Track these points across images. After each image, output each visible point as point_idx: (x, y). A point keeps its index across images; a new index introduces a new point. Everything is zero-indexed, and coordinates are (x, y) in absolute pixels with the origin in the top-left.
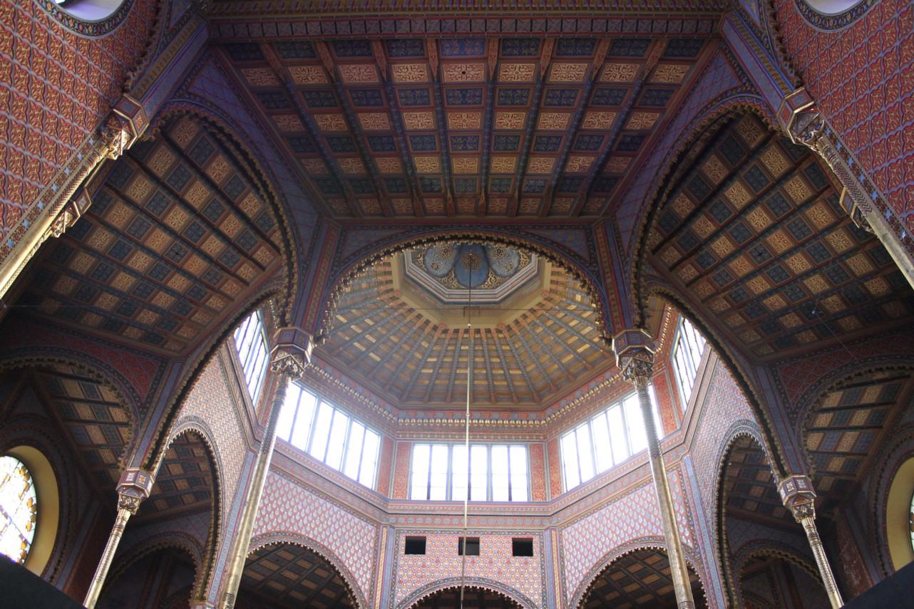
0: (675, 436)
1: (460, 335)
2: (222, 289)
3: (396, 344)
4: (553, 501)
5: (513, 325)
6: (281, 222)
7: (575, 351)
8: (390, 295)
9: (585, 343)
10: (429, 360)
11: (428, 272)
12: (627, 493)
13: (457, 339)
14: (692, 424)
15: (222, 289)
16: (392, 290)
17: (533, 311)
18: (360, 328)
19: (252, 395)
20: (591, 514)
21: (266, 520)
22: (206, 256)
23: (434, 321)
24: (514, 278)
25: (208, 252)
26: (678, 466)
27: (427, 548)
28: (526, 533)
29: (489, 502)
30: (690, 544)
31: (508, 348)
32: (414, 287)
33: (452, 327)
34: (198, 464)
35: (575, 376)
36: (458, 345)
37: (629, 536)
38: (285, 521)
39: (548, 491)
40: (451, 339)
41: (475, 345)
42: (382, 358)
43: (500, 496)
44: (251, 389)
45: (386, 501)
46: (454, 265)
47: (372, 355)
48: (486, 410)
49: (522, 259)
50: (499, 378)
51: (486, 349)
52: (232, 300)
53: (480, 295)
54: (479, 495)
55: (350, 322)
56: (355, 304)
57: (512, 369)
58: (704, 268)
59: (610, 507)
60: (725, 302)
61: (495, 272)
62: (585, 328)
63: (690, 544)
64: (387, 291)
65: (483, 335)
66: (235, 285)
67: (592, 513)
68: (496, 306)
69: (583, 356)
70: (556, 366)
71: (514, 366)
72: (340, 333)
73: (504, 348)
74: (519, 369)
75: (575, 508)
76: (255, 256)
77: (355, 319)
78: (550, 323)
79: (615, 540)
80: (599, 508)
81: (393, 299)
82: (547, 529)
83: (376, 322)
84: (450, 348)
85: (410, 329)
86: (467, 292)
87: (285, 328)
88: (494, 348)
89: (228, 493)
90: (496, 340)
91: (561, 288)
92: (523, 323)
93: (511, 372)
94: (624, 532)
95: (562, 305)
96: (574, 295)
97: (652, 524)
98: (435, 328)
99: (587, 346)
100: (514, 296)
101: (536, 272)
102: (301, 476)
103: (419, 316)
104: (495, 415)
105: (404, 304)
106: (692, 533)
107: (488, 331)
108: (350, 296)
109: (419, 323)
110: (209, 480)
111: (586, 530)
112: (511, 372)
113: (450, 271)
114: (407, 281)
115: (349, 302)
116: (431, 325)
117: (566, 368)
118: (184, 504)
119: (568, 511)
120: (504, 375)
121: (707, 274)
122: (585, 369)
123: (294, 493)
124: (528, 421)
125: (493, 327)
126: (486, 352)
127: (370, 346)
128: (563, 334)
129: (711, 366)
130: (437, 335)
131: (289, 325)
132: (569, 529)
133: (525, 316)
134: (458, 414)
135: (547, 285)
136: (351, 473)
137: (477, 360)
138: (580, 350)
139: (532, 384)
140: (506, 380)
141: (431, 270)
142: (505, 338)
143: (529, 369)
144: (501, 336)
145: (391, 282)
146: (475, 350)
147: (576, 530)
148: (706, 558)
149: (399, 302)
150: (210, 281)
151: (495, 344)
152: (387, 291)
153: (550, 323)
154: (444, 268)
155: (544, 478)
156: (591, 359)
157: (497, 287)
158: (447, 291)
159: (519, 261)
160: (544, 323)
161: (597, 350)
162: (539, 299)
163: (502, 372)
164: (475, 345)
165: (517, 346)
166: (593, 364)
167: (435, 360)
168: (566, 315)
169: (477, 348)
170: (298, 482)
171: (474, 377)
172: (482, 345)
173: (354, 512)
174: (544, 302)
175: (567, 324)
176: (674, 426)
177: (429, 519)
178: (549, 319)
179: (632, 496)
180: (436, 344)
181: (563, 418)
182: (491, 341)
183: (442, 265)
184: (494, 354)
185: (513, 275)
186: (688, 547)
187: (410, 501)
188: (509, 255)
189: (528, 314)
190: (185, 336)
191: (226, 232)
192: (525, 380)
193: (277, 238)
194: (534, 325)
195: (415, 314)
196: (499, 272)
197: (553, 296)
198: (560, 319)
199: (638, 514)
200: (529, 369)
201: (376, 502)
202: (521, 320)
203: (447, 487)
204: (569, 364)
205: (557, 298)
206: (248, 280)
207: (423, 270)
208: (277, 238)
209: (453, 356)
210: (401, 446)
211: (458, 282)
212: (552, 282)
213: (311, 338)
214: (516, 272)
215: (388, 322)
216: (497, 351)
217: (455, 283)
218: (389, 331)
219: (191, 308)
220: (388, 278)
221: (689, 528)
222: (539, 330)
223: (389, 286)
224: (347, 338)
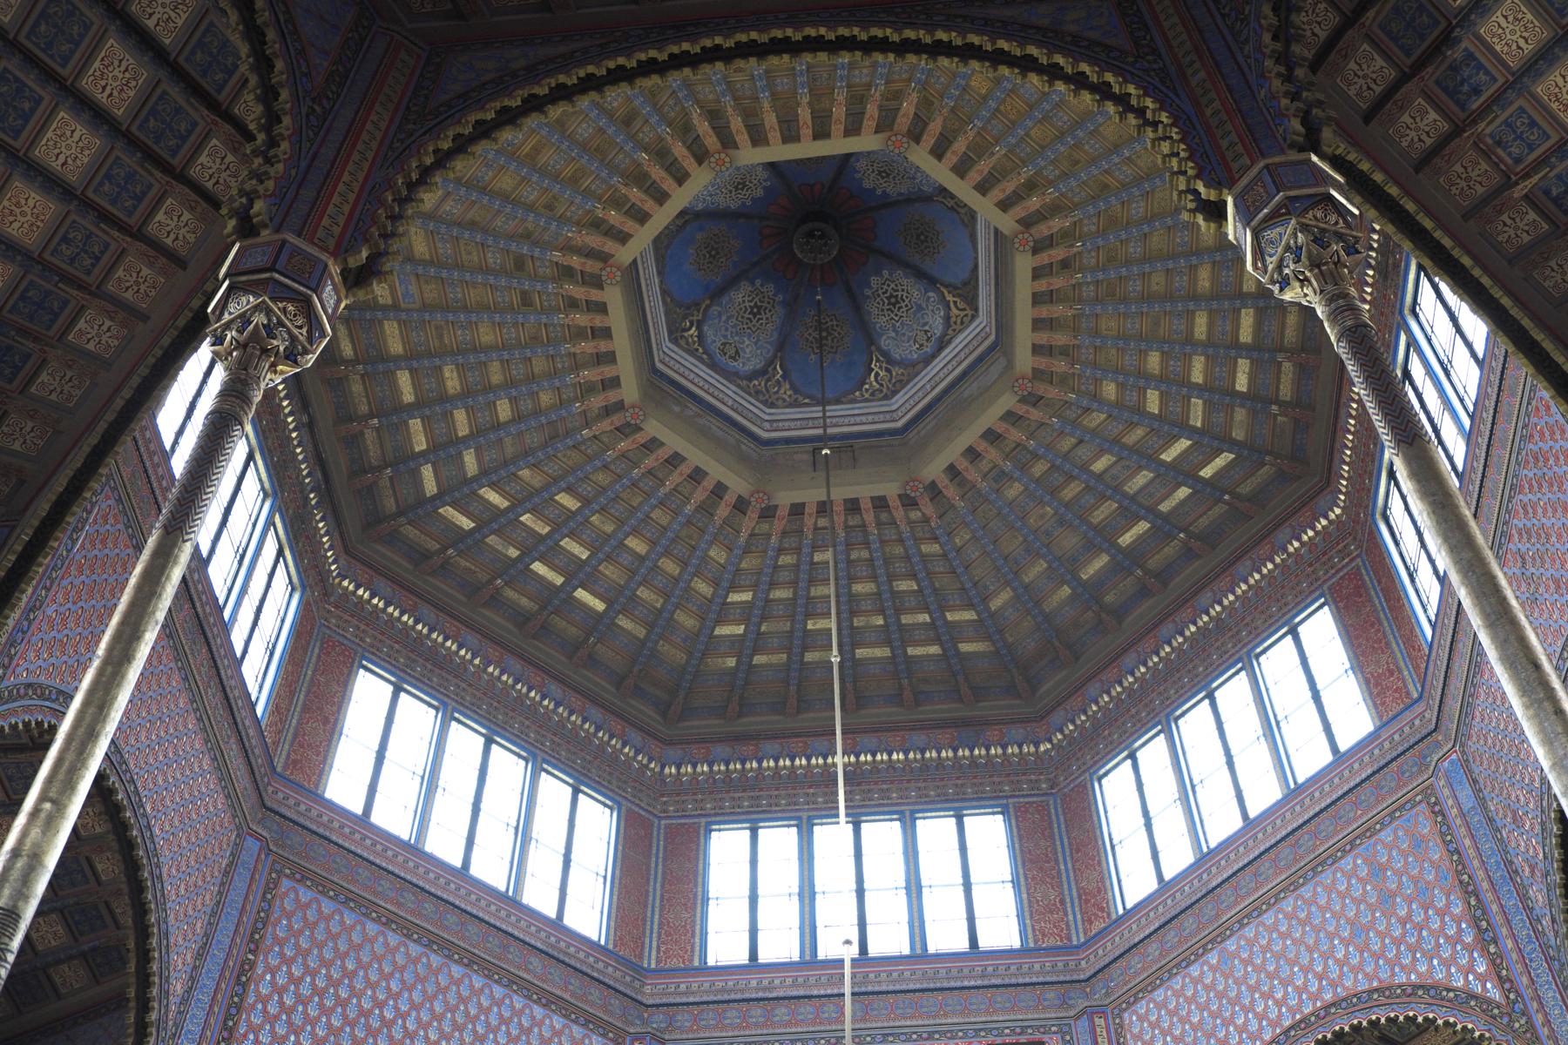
0: (1409, 716)
1: (809, 521)
2: (110, 287)
4: (1090, 941)
5: (943, 482)
6: (264, 64)
8: (617, 419)
9: (1137, 519)
10: (734, 597)
11: (714, 366)
12: (1292, 886)
14: (1455, 666)
15: (110, 287)
16: (620, 406)
18: (547, 521)
19: (253, 688)
20: (1198, 956)
21: (297, 1020)
22: (49, 181)
23: (738, 484)
24: (938, 364)
25: (56, 165)
26: (1428, 792)
27: (647, 225)
28: (1023, 1030)
29: (920, 955)
30: (1494, 993)
31: (936, 548)
34: (88, 859)
35: (1119, 613)
36: (805, 550)
37: (1314, 997)
38: (352, 1024)
39: (1074, 916)
40: (784, 533)
41: (849, 546)
42: (610, 603)
43: (947, 937)
44: (252, 670)
45: (640, 972)
46: (780, 347)
47: (581, 594)
48: (893, 728)
49: (954, 311)
52: (144, 318)
53: (849, 417)
54: (890, 940)
55: (517, 505)
56: (526, 453)
57: (952, 609)
58: (1463, 107)
59: (1249, 932)
60: (1532, 215)
61: (886, 354)
63: (1494, 993)
64: (608, 411)
65: (869, 517)
66: (145, 271)
67: (1199, 952)
69: (1135, 555)
72: (492, 540)
73: (925, 548)
75: (1153, 949)
76: (194, 172)
77: (530, 496)
78: (1039, 468)
79: (1273, 1015)
80: (1218, 938)
81: (626, 430)
82: (1083, 1012)
83: (586, 502)
84: (785, 560)
85: (676, 513)
86: (816, 411)
87: (251, 241)
89: (176, 937)
90: (903, 527)
91: (1061, 365)
92: (973, 474)
93: (949, 616)
94: (1297, 988)
95: (1071, 414)
96: (1097, 382)
97: (1376, 957)
98: (741, 506)
99: (1143, 526)
101: (993, 337)
102: (399, 905)
103: (697, 475)
104: (919, 738)
105: (653, 445)
106: (1495, 963)
107: (880, 503)
110: (123, 909)
111: (1189, 1001)
112: (949, 616)
113: (771, 362)
114: (661, 386)
116: (729, 498)
117: (1090, 593)
118: (59, 996)
119: (1135, 961)
121: (1475, 122)
122: (1144, 592)
123: (379, 948)
124: (1004, 748)
125: (890, 490)
127: (578, 574)
129: (1511, 403)
130: (748, 523)
131: (265, 233)
132: (1141, 1008)
133: (972, 454)
134: (820, 744)
135: (1024, 360)
136: (539, 897)
137: (858, 588)
141: (724, 360)
142: (926, 520)
143: (996, 604)
144: (915, 515)
146: (849, 562)
147: (1162, 1005)
148: (1548, 1023)
149: (641, 438)
150: (72, 260)
151: (901, 541)
152: (608, 411)
153: (1039, 468)
154: (752, 357)
155: (1060, 885)
156: (1154, 563)
157: (895, 393)
158: (766, 413)
159: (947, 318)
160: (1024, 468)
161: (1170, 537)
162: (1007, 402)
163: (926, 618)
166: (1163, 576)
167: (746, 596)
168: (1081, 442)
169: (854, 555)
170: (389, 921)
171: (852, 636)
173: (550, 1001)
174: (1022, 409)
175: (1085, 468)
176: (1402, 691)
177: (757, 1012)
178: (1036, 456)
179: (1306, 891)
180: (746, 551)
181: (1097, 725)
182: (890, 534)
183: (748, 346)
184: (900, 567)
185: (934, 356)
186: (1489, 1001)
187: (705, 970)
189: (982, 446)
190: (17, 446)
191: (102, 98)
193: (250, 109)
194: (1001, 477)
195: (685, 469)
196: (896, 354)
197: (1042, 389)
198: (1066, 456)
199: (1331, 936)
200: (996, 604)
201: (611, 974)
202: (962, 465)
203: (802, 928)
204: (1099, 582)
206: (183, 252)
208: (250, 109)
210: (672, 834)
212: (1037, 349)
213: (335, 269)
214: (940, 349)
215: (617, 498)
216: (908, 558)
217: (786, 391)
219: (26, 357)
221: (1484, 951)
222: (1014, 491)
223: (612, 396)
224: (513, 553)
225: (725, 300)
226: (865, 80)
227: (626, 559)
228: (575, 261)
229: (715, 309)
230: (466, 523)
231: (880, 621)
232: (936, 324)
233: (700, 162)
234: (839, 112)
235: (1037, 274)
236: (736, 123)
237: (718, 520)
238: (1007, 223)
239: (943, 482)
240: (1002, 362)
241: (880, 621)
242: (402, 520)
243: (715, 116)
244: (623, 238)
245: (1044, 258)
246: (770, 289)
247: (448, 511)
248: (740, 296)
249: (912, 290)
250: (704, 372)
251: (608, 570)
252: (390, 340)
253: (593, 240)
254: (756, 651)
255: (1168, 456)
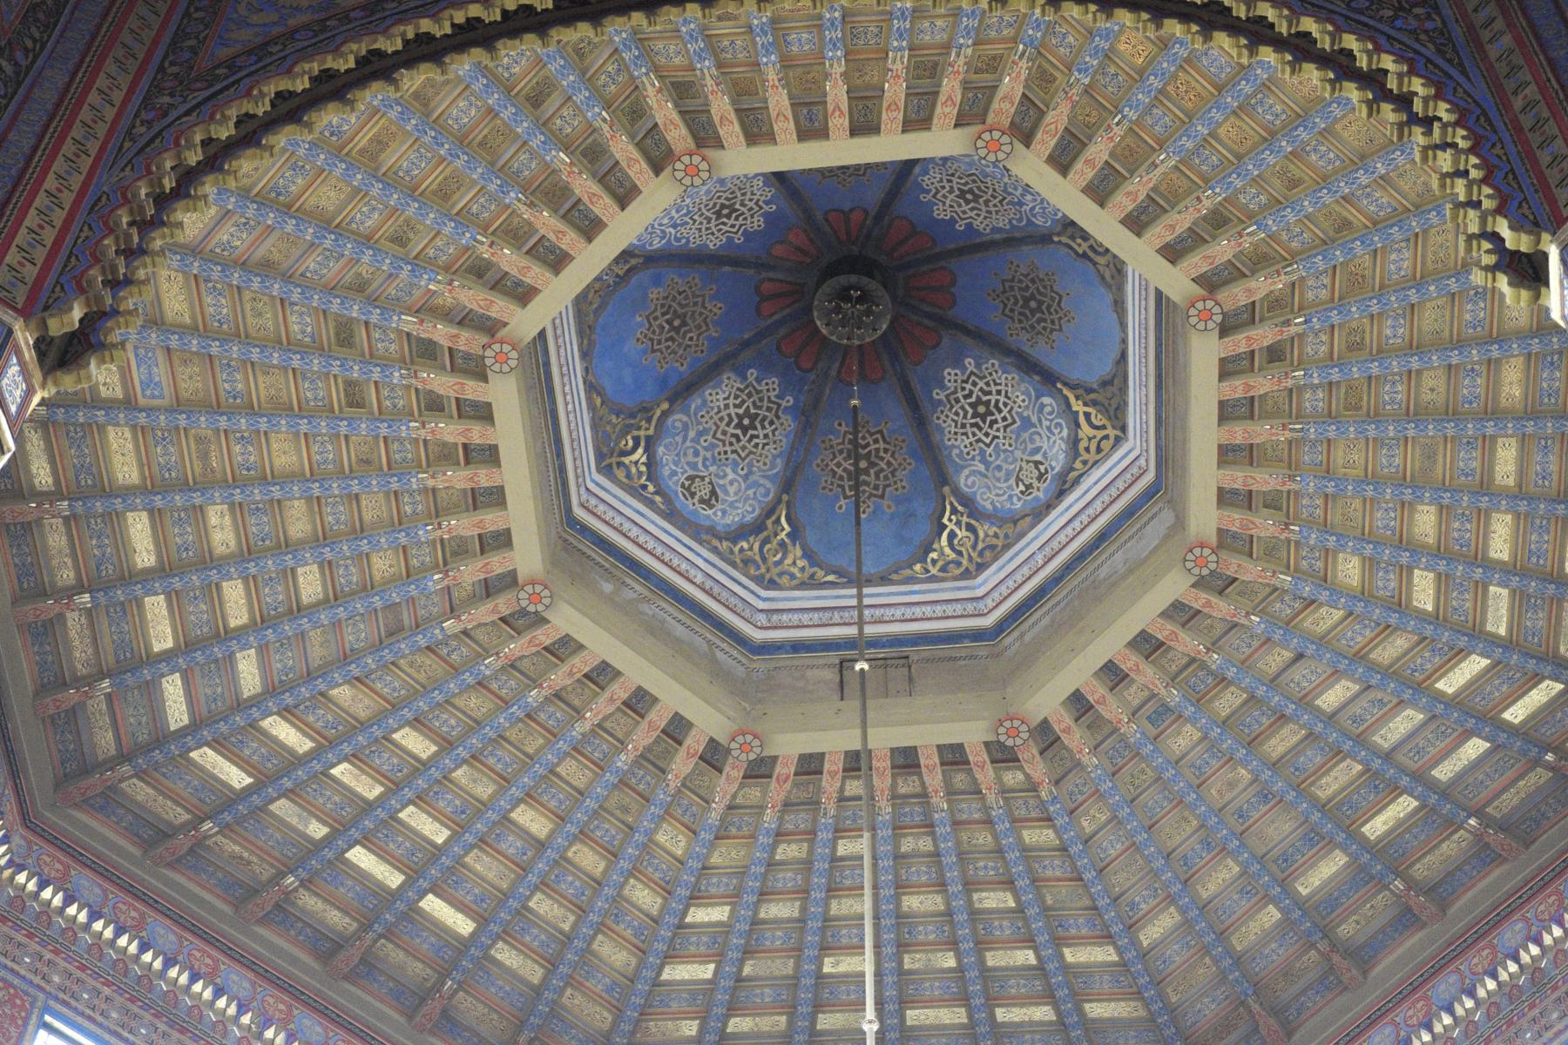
1: (830, 784)
3: (541, 845)
5: (1062, 721)
7: (1354, 836)
8: (504, 604)
10: (698, 915)
11: (671, 514)
13: (814, 804)
16: (510, 580)
17: (1146, 644)
24: (1056, 519)
32: (609, 575)
33: (789, 745)
35: (1362, 956)
40: (787, 805)
41: (898, 828)
46: (787, 485)
49: (1086, 430)
50: (1014, 987)
51: (958, 903)
55: (328, 746)
56: (346, 658)
61: (968, 501)
62: (1384, 719)
64: (489, 589)
65: (934, 779)
68: (981, 648)
70: (1271, 915)
71: (1079, 924)
74: (1107, 938)
78: (1228, 702)
81: (520, 622)
86: (847, 597)
88: (983, 838)
91: (1265, 526)
92: (1112, 708)
93: (1069, 955)
98: (713, 756)
99: (1405, 805)
100: (1061, 593)
101: (1150, 476)
103: (639, 702)
105: (564, 648)
107: (954, 756)
108: (324, 618)
109: (643, 736)
112: (1069, 955)
113: (770, 511)
115: (317, 651)
116: (695, 742)
120: (1040, 969)
122: (1406, 919)
126: (961, 917)
128: (1295, 750)
130: (726, 786)
133: (1113, 674)
135: (1204, 517)
137: (912, 902)
138: (1376, 827)
139: (1171, 1010)
140: (1049, 997)
141: (689, 506)
143: (1150, 934)
144: (1012, 778)
145: (502, 540)
146: (898, 857)
149: (544, 636)
152: (489, 589)
153: (1228, 702)
156: (1425, 868)
157: (981, 567)
158: (763, 598)
159: (1074, 442)
160: (1200, 700)
161: (1452, 825)
162: (1174, 586)
163: (1027, 957)
164: (898, 828)
165: (1087, 826)
166: (1440, 892)
169: (907, 845)
172: (929, 826)
174: (1198, 600)
175: (1305, 702)
178: (1222, 681)
182: (969, 809)
183: (731, 481)
185: (1049, 506)
188: (1027, 423)
189: (1131, 661)
192: (1138, 995)
196: (985, 501)
197: (1234, 565)
200: (1150, 934)
202: (1097, 692)
204: (1330, 903)
205: (1249, 571)
207: (650, 503)
209: (804, 892)
211: (808, 554)
212: (1225, 497)
213: (24, 337)
214: (1061, 494)
218: (505, 781)
220: (491, 520)
222: (1184, 739)
223: (497, 564)
224: (317, 830)
225: (695, 403)
226: (940, 37)
227: (512, 845)
228: (441, 333)
229: (677, 419)
230: (237, 778)
231: (950, 961)
232: (1055, 452)
233: (657, 169)
234: (895, 91)
235: (1227, 369)
236: (721, 106)
237: (673, 781)
238: (1177, 282)
239: (1062, 721)
240: (1167, 517)
241: (950, 961)
242: (126, 769)
243: (683, 91)
244: (524, 295)
245: (1239, 343)
246: (771, 386)
247: (207, 757)
248: (721, 396)
249: (1015, 392)
250: (655, 524)
251: (482, 864)
252: (117, 460)
253: (472, 297)
254: (732, 1009)
255: (1450, 684)
